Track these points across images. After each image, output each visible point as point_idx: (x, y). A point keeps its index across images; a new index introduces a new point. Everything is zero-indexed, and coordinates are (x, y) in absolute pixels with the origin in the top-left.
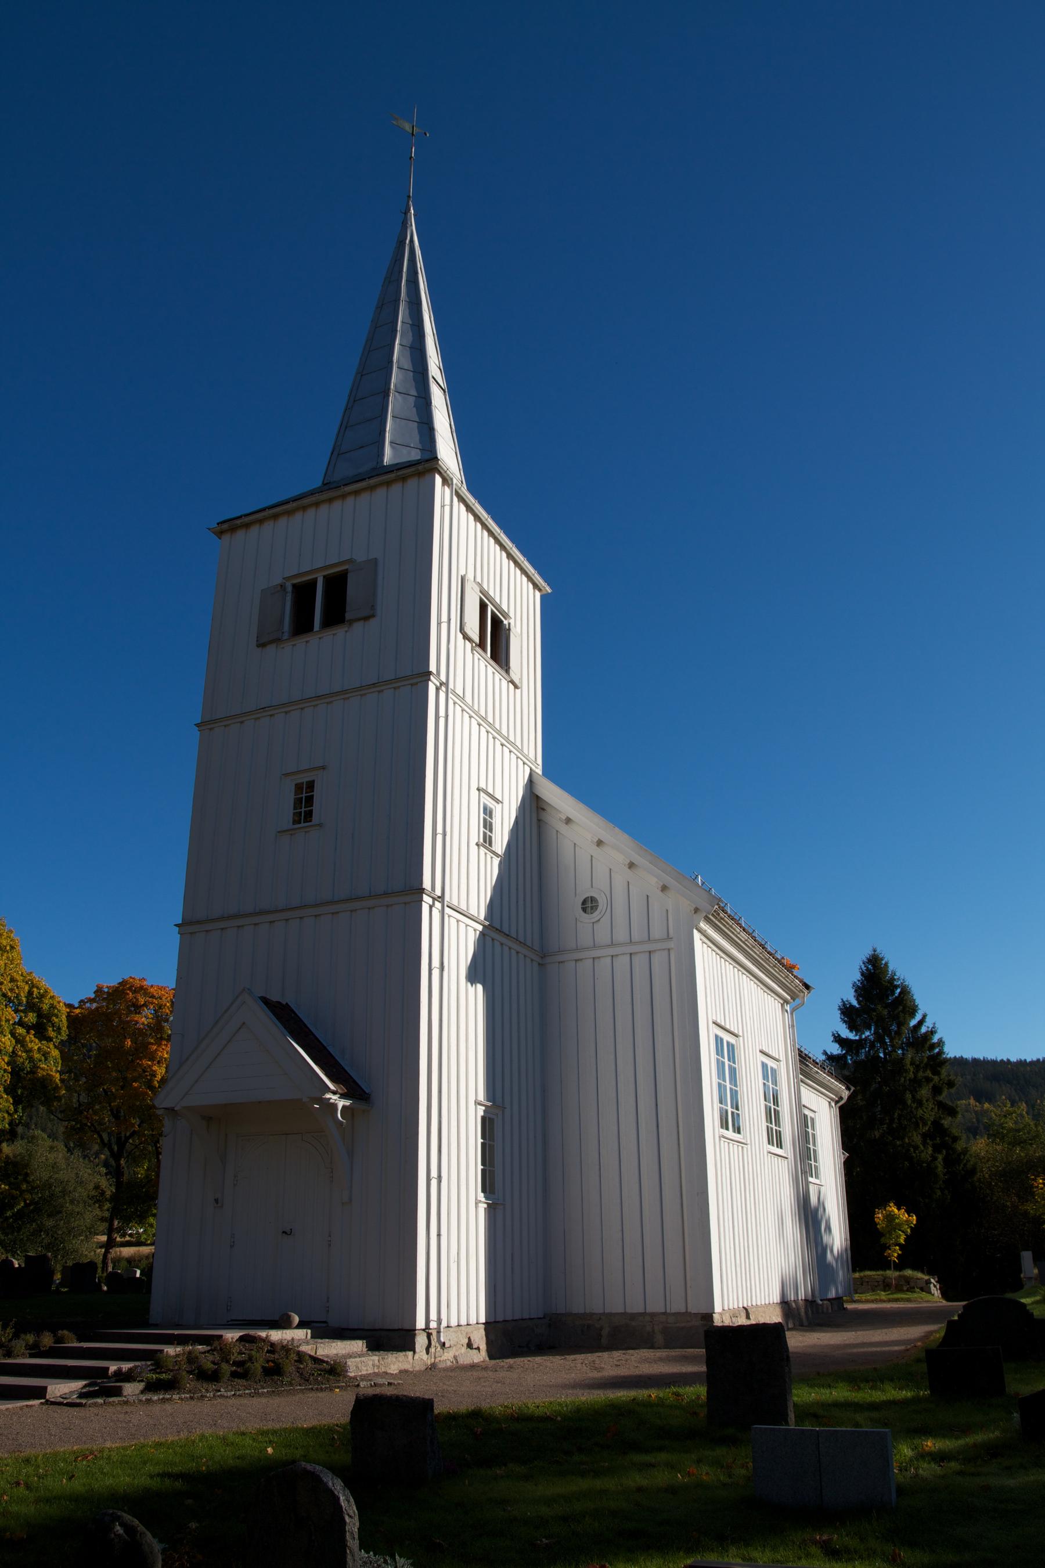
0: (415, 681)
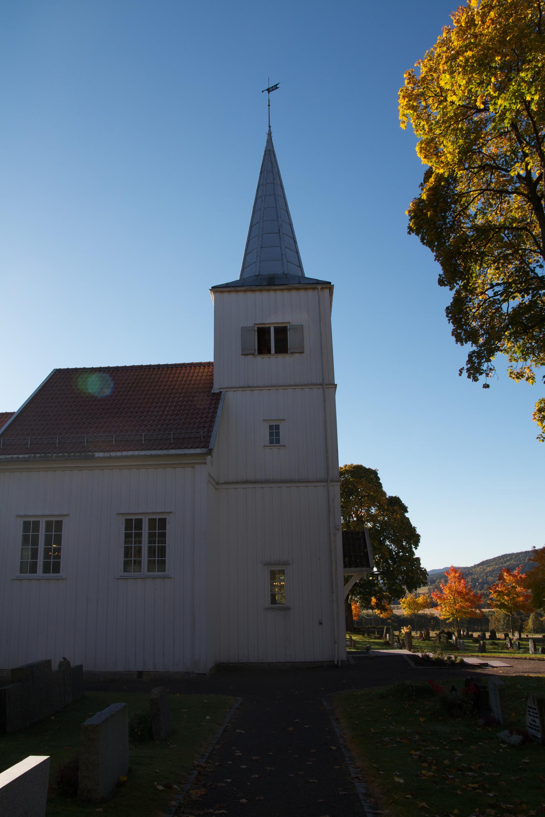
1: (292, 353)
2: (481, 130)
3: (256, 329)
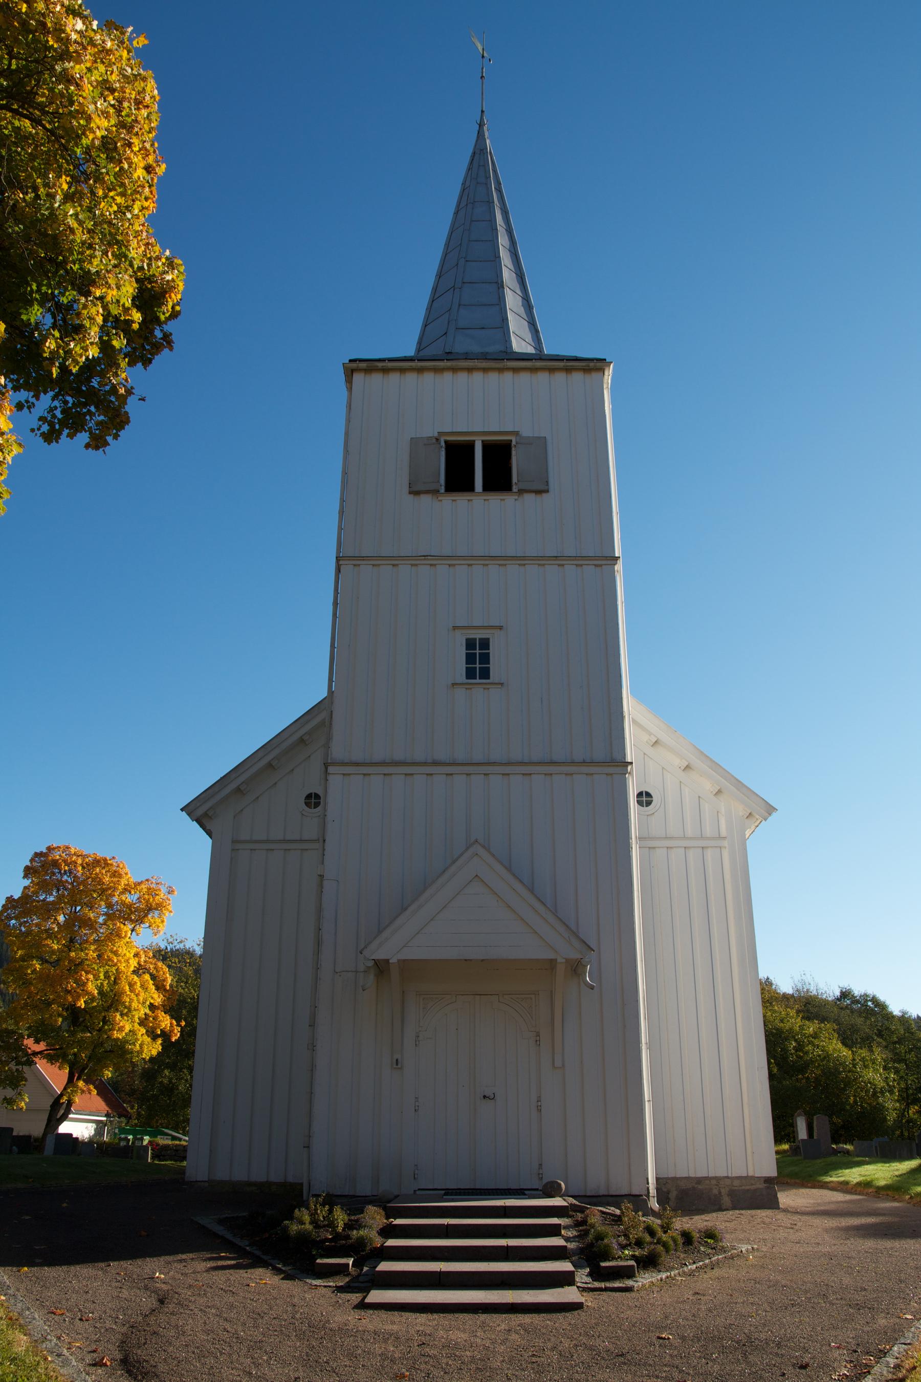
0: (487, 562)
1: (521, 492)
3: (443, 444)
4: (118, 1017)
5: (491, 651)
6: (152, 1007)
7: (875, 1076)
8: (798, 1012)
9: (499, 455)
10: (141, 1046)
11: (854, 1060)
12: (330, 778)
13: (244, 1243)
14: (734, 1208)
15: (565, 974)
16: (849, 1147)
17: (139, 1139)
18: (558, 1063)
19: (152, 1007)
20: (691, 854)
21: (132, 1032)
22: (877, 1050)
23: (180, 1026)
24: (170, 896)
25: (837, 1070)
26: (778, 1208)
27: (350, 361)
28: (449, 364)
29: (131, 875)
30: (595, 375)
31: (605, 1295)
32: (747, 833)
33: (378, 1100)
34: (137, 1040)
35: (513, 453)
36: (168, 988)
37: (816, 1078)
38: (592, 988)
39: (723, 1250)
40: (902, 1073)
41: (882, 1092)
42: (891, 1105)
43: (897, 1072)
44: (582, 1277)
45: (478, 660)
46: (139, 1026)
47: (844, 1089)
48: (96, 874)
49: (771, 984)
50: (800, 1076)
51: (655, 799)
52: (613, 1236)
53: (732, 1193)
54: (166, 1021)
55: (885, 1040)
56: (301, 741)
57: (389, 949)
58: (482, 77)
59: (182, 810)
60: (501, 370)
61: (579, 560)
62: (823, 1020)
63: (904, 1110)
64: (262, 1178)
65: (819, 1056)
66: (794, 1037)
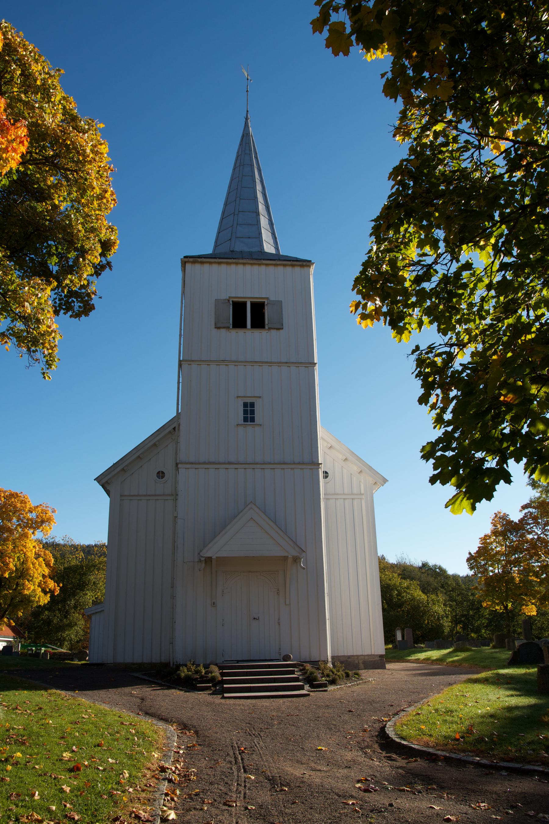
1: (270, 329)
2: (488, 110)
3: (231, 303)
4: (27, 582)
5: (255, 408)
6: (44, 576)
7: (439, 609)
8: (399, 575)
9: (259, 308)
10: (39, 598)
11: (428, 600)
12: (180, 470)
13: (160, 682)
14: (365, 669)
15: (291, 564)
16: (422, 645)
17: (39, 649)
18: (288, 603)
19: (44, 576)
20: (347, 501)
21: (34, 590)
22: (440, 595)
23: (59, 586)
24: (53, 514)
25: (419, 606)
26: (385, 668)
27: (185, 257)
28: (234, 261)
29: (32, 503)
30: (306, 269)
31: (317, 693)
32: (374, 492)
33: (210, 621)
34: (36, 594)
35: (266, 308)
36: (52, 565)
37: (408, 611)
38: (304, 569)
39: (362, 679)
40: (454, 607)
41: (442, 618)
42: (447, 624)
43: (451, 606)
44: (307, 687)
45: (249, 413)
46: (38, 588)
47: (422, 616)
48: (12, 502)
49: (384, 559)
50: (399, 610)
51: (330, 475)
52: (313, 676)
53: (364, 663)
54: (51, 584)
55: (445, 589)
56: (155, 444)
57: (211, 552)
58: (247, 91)
59: (95, 480)
60: (259, 265)
61: (298, 364)
62: (412, 579)
63: (454, 627)
64: (140, 661)
65: (410, 598)
66: (396, 588)
